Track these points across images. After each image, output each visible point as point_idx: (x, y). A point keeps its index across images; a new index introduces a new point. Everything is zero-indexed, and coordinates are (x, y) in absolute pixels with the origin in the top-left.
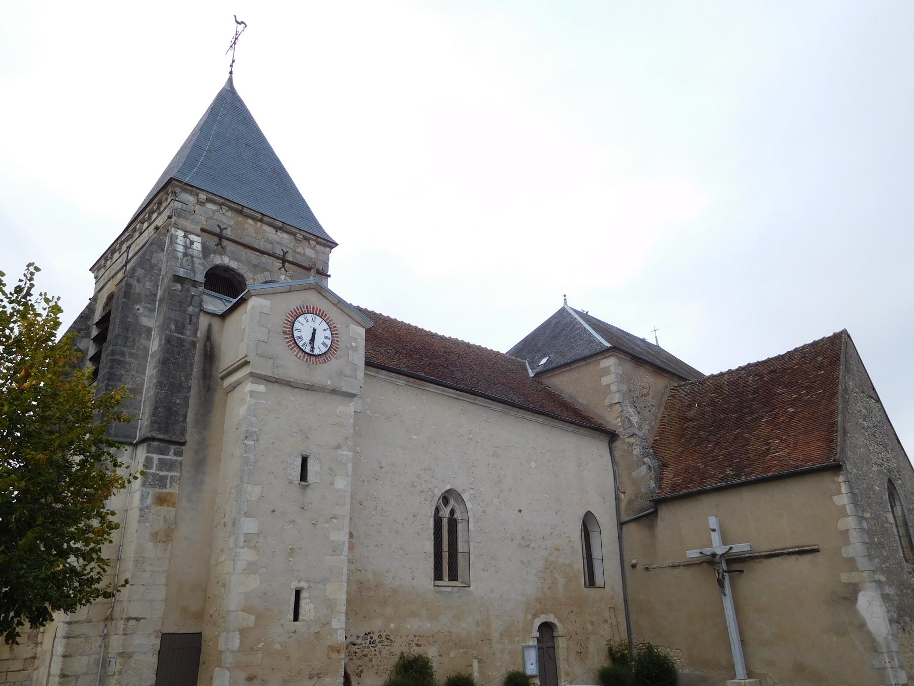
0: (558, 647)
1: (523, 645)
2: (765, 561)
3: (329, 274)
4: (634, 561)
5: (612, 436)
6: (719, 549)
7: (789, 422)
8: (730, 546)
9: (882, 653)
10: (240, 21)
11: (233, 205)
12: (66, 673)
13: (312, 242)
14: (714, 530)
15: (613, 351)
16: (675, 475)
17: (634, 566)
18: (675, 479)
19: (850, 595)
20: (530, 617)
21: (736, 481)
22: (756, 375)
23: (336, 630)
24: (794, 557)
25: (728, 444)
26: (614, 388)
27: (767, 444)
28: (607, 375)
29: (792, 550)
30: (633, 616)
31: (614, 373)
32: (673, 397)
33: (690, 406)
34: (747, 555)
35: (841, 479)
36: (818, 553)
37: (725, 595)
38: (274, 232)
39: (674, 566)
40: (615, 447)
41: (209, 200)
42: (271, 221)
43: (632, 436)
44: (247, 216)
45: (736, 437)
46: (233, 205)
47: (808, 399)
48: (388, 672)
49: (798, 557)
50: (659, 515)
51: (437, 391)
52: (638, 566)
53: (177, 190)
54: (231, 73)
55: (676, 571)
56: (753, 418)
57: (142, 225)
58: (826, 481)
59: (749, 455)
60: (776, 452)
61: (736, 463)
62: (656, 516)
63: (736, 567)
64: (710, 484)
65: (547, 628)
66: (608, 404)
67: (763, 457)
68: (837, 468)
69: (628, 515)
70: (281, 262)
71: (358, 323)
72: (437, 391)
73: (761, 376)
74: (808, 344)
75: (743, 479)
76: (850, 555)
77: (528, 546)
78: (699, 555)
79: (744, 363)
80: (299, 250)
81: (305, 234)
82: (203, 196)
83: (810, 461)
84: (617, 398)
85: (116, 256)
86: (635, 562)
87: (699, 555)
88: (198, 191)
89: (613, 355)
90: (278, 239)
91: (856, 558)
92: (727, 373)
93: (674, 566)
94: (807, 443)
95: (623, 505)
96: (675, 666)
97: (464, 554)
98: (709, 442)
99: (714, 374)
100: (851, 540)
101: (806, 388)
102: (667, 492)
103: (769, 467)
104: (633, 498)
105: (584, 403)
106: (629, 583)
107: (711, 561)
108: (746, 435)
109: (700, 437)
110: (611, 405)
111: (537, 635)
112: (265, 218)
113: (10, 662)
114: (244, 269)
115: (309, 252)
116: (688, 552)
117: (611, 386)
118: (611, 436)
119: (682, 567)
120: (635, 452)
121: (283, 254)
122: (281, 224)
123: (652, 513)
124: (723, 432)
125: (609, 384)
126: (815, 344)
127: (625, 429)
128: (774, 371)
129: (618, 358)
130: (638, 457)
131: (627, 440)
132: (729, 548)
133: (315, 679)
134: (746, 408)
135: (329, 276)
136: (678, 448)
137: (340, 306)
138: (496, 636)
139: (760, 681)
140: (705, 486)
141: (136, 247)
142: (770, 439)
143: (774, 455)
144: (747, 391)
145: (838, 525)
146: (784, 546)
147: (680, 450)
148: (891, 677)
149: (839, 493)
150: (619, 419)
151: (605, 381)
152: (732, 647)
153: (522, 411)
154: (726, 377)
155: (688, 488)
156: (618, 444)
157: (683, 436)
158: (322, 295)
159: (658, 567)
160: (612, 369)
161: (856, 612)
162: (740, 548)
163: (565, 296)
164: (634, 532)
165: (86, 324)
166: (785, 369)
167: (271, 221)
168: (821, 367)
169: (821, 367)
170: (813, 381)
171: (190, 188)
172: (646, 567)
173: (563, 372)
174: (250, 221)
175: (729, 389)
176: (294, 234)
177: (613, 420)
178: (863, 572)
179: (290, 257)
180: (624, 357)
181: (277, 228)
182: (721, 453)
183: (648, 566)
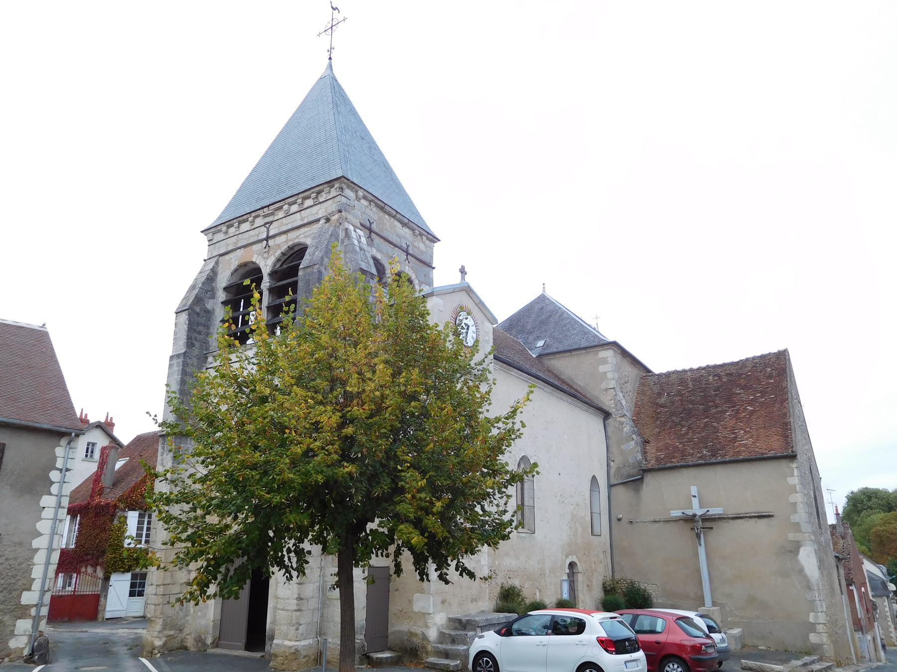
0: (578, 581)
1: (561, 579)
2: (731, 522)
3: (433, 266)
4: (620, 516)
5: (606, 415)
6: (697, 510)
7: (749, 417)
8: (708, 509)
9: (813, 590)
10: (334, 7)
11: (379, 202)
12: (302, 597)
13: (424, 238)
14: (695, 496)
15: (612, 346)
16: (657, 451)
17: (619, 520)
18: (658, 454)
19: (794, 549)
20: (564, 558)
21: (713, 460)
22: (715, 375)
23: (483, 565)
24: (754, 520)
25: (699, 429)
26: (609, 375)
27: (734, 433)
28: (605, 364)
29: (753, 514)
30: (616, 559)
31: (611, 363)
32: (643, 384)
33: (660, 395)
34: (717, 517)
35: (795, 465)
36: (772, 518)
37: (700, 545)
38: (401, 227)
39: (655, 521)
40: (608, 424)
41: (365, 198)
42: (401, 217)
43: (623, 416)
44: (386, 212)
45: (706, 425)
46: (379, 202)
47: (764, 401)
48: (496, 598)
49: (757, 520)
50: (645, 481)
51: (516, 375)
52: (623, 520)
53: (344, 186)
54: (330, 58)
55: (657, 525)
56: (718, 411)
57: (289, 207)
58: (783, 465)
59: (720, 440)
60: (743, 441)
61: (710, 445)
62: (642, 482)
63: (708, 525)
64: (691, 460)
65: (572, 565)
66: (604, 388)
67: (732, 443)
68: (793, 457)
69: (617, 479)
70: (406, 254)
71: (489, 320)
72: (516, 375)
73: (720, 377)
74: (758, 357)
75: (719, 459)
76: (797, 521)
77: (563, 502)
78: (681, 515)
79: (704, 365)
80: (416, 244)
81: (421, 230)
82: (361, 193)
83: (772, 450)
84: (612, 384)
85: (245, 226)
86: (621, 517)
87: (681, 515)
88: (358, 189)
89: (612, 348)
90: (404, 234)
91: (801, 523)
92: (689, 370)
93: (655, 521)
94: (767, 436)
95: (613, 471)
96: (652, 596)
97: (529, 507)
98: (683, 426)
99: (678, 370)
100: (798, 509)
101: (761, 392)
102: (652, 463)
103: (739, 451)
104: (621, 466)
105: (582, 385)
106: (614, 532)
107: (690, 520)
108: (715, 424)
109: (673, 422)
110: (607, 389)
111: (568, 571)
112: (398, 215)
113: (171, 586)
114: (385, 260)
115: (419, 246)
116: (671, 512)
117: (607, 374)
118: (606, 415)
119: (661, 522)
120: (625, 429)
121: (406, 247)
122: (406, 221)
123: (639, 479)
124: (693, 419)
125: (606, 372)
126: (763, 357)
127: (617, 410)
128: (731, 375)
129: (614, 351)
130: (627, 434)
131: (619, 419)
132: (706, 511)
133: (474, 602)
134: (710, 401)
135: (434, 268)
136: (655, 428)
137: (480, 306)
138: (547, 572)
139: (721, 608)
140: (688, 462)
141: (281, 226)
142: (736, 430)
143: (741, 442)
144: (709, 388)
145: (789, 499)
146: (747, 512)
147: (657, 430)
148: (819, 607)
149: (793, 476)
150: (613, 402)
151: (602, 368)
152: (703, 584)
153: (562, 393)
154: (689, 373)
155: (672, 462)
156: (610, 421)
157: (658, 418)
158: (470, 296)
159: (641, 522)
160: (610, 360)
161: (797, 561)
162: (715, 511)
163: (544, 284)
164: (621, 493)
165: (211, 286)
166: (740, 374)
167: (401, 217)
168: (770, 377)
169: (770, 377)
170: (766, 387)
171: (353, 186)
172: (631, 521)
173: (563, 356)
174: (387, 216)
175: (692, 384)
176: (413, 230)
177: (607, 402)
178: (805, 533)
179: (411, 252)
180: (617, 350)
181: (404, 225)
182: (695, 437)
183: (633, 521)
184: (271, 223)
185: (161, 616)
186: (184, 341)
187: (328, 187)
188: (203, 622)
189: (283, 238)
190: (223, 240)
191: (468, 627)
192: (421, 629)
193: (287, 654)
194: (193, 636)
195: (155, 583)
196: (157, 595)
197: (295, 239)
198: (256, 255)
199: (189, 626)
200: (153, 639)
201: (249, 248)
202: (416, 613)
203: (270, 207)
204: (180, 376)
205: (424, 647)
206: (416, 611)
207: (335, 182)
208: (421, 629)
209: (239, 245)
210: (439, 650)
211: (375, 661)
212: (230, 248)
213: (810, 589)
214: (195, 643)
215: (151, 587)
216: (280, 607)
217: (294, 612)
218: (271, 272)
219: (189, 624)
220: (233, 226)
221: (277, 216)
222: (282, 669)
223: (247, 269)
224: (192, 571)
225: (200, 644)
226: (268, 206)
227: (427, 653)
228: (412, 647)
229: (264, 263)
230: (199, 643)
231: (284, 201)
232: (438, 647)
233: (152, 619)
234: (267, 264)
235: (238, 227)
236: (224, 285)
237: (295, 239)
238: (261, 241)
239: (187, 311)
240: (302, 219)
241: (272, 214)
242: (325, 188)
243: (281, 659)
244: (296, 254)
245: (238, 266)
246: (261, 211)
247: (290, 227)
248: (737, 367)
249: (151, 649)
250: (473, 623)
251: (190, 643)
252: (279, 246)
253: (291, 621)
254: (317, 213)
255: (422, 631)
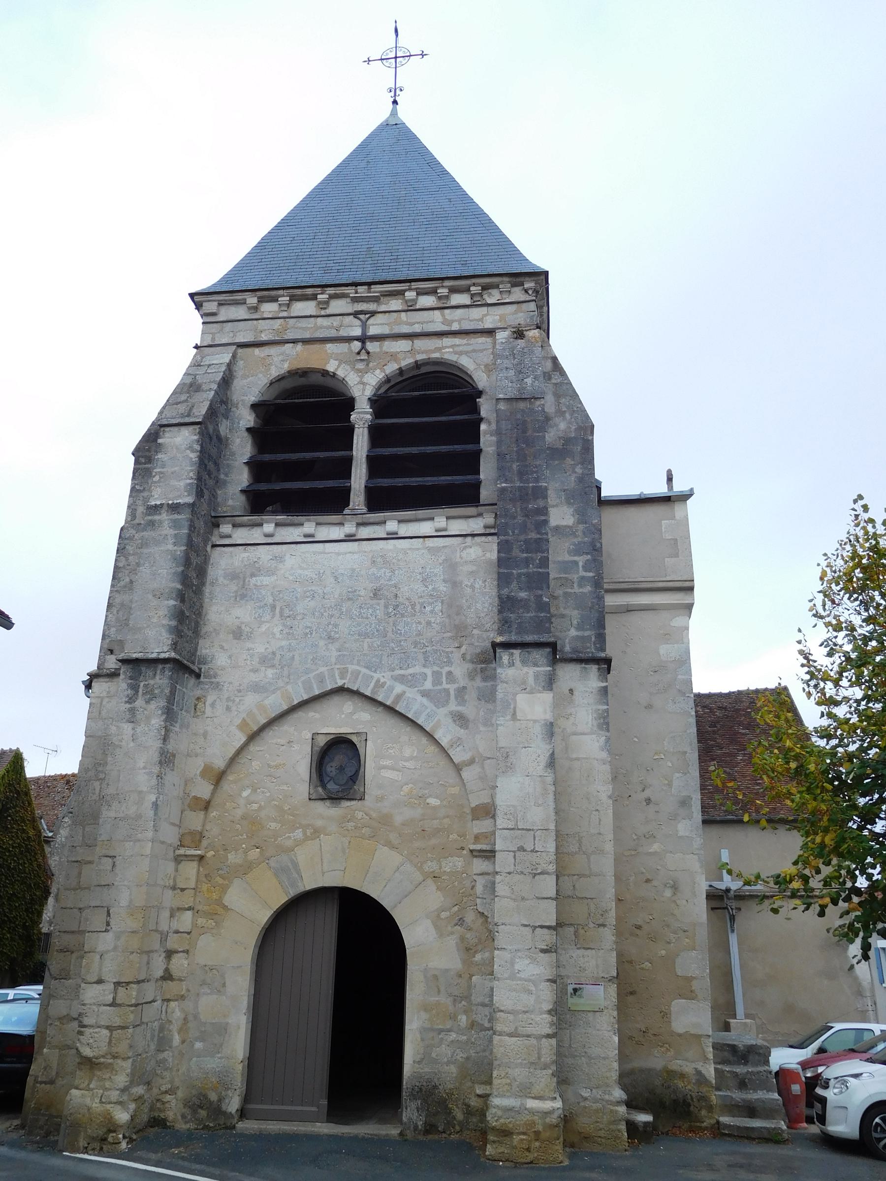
85: (302, 308)
128: (725, 708)
141: (401, 323)
166: (737, 709)
184: (373, 313)
185: (130, 1054)
186: (189, 481)
187: (509, 282)
188: (212, 1064)
189: (403, 345)
190: (245, 320)
191: (751, 1057)
192: (694, 1065)
193: (540, 1128)
194: (180, 1094)
195: (111, 978)
196: (120, 1005)
197: (434, 351)
198: (337, 363)
199: (167, 1074)
200: (108, 1106)
201: (316, 347)
202: (680, 1035)
203: (372, 287)
204: (184, 548)
205: (703, 1098)
206: (681, 1030)
207: (527, 279)
208: (694, 1065)
209: (290, 336)
210: (733, 1103)
211: (641, 1129)
212: (264, 337)
213: (861, 995)
214: (187, 1111)
215: (99, 987)
216: (506, 1029)
217: (544, 1040)
218: (374, 395)
219: (166, 1069)
220: (277, 301)
221: (383, 306)
222: (528, 1160)
223: (302, 381)
224: (177, 952)
225: (203, 1113)
226: (369, 284)
227: (710, 1108)
228: (675, 1098)
229: (358, 379)
230: (200, 1111)
231: (409, 284)
232: (732, 1097)
233: (102, 1060)
234: (365, 380)
235: (288, 306)
236: (253, 398)
237: (434, 351)
238: (349, 339)
239: (197, 427)
240: (445, 322)
241: (376, 300)
242: (502, 282)
243: (522, 1140)
244: (418, 378)
245: (289, 372)
246: (349, 288)
247: (417, 329)
248: (730, 701)
249: (105, 1130)
250: (761, 1051)
251: (174, 1110)
252: (393, 356)
253: (539, 1058)
254: (481, 320)
255: (696, 1069)
